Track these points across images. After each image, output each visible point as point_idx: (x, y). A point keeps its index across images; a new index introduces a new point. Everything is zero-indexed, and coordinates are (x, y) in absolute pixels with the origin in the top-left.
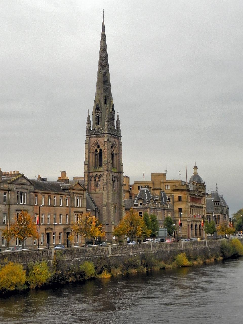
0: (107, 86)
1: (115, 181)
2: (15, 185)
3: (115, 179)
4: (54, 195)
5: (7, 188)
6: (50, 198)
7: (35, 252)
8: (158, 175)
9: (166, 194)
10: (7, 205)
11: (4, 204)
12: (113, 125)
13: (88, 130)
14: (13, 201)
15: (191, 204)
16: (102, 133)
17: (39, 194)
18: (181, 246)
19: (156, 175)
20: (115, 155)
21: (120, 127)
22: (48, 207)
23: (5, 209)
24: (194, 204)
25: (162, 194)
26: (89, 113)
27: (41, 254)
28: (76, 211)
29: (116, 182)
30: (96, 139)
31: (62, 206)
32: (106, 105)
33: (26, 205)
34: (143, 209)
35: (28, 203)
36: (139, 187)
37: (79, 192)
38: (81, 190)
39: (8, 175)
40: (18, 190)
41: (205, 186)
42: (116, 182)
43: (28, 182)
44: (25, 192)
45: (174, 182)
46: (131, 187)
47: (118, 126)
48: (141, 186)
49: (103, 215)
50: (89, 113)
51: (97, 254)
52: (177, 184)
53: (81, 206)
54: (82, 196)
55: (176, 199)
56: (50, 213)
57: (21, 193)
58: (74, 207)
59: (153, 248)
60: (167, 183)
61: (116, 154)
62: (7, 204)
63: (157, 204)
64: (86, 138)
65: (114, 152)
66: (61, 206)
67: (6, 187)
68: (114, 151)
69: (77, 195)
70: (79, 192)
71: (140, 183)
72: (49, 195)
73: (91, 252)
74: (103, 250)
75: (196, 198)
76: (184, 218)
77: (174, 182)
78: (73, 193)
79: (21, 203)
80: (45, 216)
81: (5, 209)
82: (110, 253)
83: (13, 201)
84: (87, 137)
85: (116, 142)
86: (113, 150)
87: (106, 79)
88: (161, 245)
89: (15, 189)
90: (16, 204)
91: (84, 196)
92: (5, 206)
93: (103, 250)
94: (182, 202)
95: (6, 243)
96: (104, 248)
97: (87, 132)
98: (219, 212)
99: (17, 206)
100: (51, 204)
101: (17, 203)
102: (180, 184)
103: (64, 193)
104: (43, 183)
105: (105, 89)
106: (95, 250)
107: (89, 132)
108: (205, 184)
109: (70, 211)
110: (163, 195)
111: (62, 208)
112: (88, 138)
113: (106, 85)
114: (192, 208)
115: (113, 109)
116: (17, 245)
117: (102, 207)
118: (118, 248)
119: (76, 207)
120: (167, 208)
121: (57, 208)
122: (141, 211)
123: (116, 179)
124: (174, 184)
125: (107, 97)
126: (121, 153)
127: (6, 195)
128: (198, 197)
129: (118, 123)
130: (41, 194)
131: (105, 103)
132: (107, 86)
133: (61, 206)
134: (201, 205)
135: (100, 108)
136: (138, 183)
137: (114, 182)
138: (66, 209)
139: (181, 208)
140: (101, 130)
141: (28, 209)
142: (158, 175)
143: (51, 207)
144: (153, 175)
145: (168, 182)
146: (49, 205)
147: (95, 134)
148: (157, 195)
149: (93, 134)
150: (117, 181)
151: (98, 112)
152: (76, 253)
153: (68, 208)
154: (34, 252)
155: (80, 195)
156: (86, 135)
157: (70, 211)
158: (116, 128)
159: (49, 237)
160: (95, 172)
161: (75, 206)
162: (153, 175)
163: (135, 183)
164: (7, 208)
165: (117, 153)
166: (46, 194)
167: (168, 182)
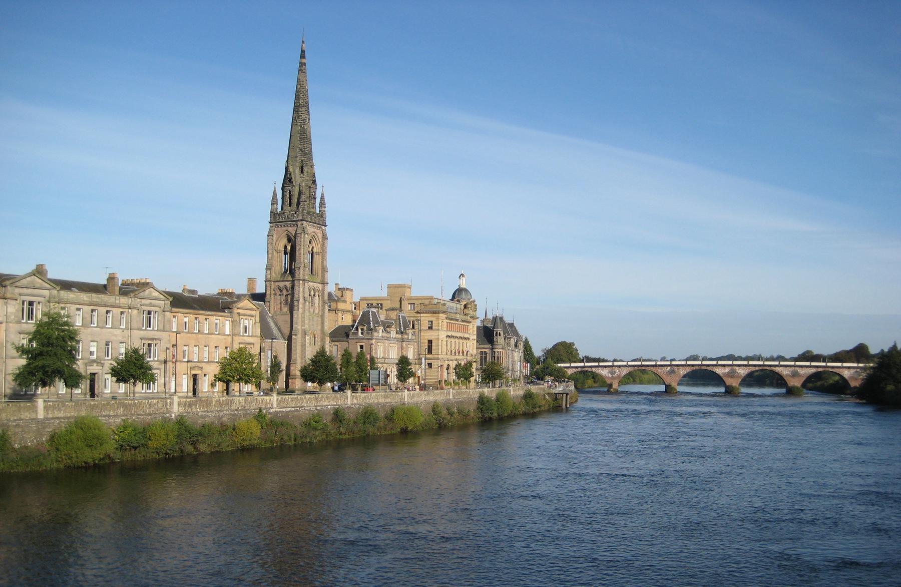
0: (306, 145)
1: (314, 295)
2: (139, 300)
3: (314, 293)
4: (205, 317)
5: (125, 304)
6: (199, 322)
7: (145, 402)
8: (398, 287)
9: (408, 317)
10: (125, 331)
11: (121, 329)
12: (314, 207)
13: (273, 214)
14: (135, 325)
15: (450, 334)
16: (295, 219)
17: (180, 314)
18: (404, 397)
19: (395, 287)
20: (315, 255)
21: (325, 211)
22: (194, 335)
23: (123, 337)
24: (454, 334)
25: (401, 317)
26: (275, 187)
27: (155, 404)
28: (243, 341)
29: (317, 298)
30: (285, 229)
31: (219, 334)
32: (302, 175)
33: (158, 330)
34: (364, 340)
35: (161, 327)
36: (368, 304)
37: (249, 312)
38: (252, 310)
39: (133, 284)
40: (144, 308)
41: (476, 305)
42: (317, 298)
43: (162, 296)
44: (156, 312)
45: (421, 299)
46: (355, 305)
47: (323, 209)
48: (372, 304)
49: (476, 341)
50: (275, 187)
51: (252, 408)
52: (427, 302)
53: (251, 335)
54: (253, 318)
55: (425, 325)
56: (197, 344)
57: (149, 313)
58: (240, 336)
59: (352, 399)
60: (411, 299)
61: (318, 253)
62: (127, 328)
63: (390, 333)
64: (271, 227)
65: (315, 250)
66: (217, 334)
67: (125, 303)
68: (315, 249)
69: (244, 317)
70: (249, 312)
71: (370, 300)
72: (197, 316)
73: (241, 404)
74: (262, 402)
75: (458, 324)
76: (436, 355)
77: (421, 299)
78: (238, 313)
79: (150, 327)
80: (190, 348)
81: (123, 337)
82: (275, 405)
83: (135, 325)
84: (271, 225)
85: (318, 234)
86: (313, 248)
87: (304, 134)
88: (367, 395)
89: (139, 306)
90: (142, 330)
91: (257, 319)
92: (123, 331)
93: (262, 402)
94: (434, 330)
95: (125, 388)
96: (264, 399)
97: (272, 217)
98: (500, 346)
99: (142, 332)
100: (199, 331)
101: (143, 327)
102: (430, 302)
103: (222, 314)
104: (190, 297)
105: (301, 150)
106: (249, 401)
107: (275, 218)
108: (475, 303)
109: (232, 342)
110: (401, 320)
111: (219, 337)
112: (272, 227)
113: (304, 142)
114: (449, 340)
115: (314, 182)
116: (144, 391)
117: (90, 343)
118: (289, 398)
119: (243, 336)
120: (408, 339)
121: (210, 336)
122: (361, 344)
123: (317, 294)
124: (423, 301)
125: (304, 162)
126: (60, 280)
127: (125, 316)
128: (462, 323)
129: (322, 204)
130: (182, 315)
131: (302, 172)
132: (306, 145)
133: (217, 334)
134: (466, 336)
135: (293, 180)
136: (366, 300)
137: (312, 297)
138: (225, 339)
139: (431, 341)
140: (293, 215)
141: (161, 337)
142: (398, 287)
143: (200, 336)
144: (389, 287)
145: (413, 299)
146: (197, 332)
147: (284, 220)
148: (392, 320)
149: (281, 220)
150: (319, 296)
151: (290, 186)
152: (215, 405)
153: (230, 337)
154: (144, 401)
155: (249, 318)
156: (270, 223)
157: (232, 342)
158: (318, 212)
159: (197, 381)
160: (282, 281)
161: (242, 334)
162: (389, 287)
163: (362, 299)
164: (127, 336)
165: (319, 251)
166: (191, 315)
167: (413, 299)
